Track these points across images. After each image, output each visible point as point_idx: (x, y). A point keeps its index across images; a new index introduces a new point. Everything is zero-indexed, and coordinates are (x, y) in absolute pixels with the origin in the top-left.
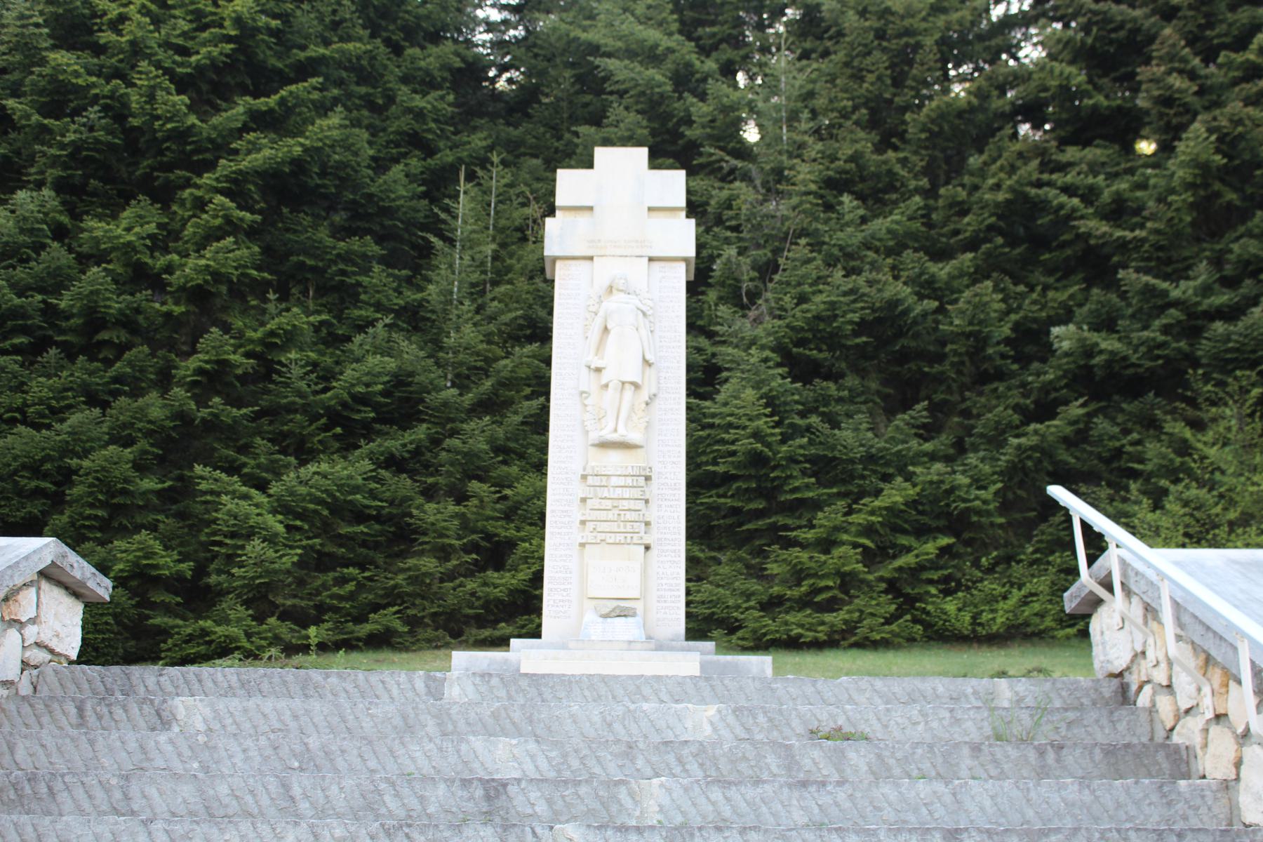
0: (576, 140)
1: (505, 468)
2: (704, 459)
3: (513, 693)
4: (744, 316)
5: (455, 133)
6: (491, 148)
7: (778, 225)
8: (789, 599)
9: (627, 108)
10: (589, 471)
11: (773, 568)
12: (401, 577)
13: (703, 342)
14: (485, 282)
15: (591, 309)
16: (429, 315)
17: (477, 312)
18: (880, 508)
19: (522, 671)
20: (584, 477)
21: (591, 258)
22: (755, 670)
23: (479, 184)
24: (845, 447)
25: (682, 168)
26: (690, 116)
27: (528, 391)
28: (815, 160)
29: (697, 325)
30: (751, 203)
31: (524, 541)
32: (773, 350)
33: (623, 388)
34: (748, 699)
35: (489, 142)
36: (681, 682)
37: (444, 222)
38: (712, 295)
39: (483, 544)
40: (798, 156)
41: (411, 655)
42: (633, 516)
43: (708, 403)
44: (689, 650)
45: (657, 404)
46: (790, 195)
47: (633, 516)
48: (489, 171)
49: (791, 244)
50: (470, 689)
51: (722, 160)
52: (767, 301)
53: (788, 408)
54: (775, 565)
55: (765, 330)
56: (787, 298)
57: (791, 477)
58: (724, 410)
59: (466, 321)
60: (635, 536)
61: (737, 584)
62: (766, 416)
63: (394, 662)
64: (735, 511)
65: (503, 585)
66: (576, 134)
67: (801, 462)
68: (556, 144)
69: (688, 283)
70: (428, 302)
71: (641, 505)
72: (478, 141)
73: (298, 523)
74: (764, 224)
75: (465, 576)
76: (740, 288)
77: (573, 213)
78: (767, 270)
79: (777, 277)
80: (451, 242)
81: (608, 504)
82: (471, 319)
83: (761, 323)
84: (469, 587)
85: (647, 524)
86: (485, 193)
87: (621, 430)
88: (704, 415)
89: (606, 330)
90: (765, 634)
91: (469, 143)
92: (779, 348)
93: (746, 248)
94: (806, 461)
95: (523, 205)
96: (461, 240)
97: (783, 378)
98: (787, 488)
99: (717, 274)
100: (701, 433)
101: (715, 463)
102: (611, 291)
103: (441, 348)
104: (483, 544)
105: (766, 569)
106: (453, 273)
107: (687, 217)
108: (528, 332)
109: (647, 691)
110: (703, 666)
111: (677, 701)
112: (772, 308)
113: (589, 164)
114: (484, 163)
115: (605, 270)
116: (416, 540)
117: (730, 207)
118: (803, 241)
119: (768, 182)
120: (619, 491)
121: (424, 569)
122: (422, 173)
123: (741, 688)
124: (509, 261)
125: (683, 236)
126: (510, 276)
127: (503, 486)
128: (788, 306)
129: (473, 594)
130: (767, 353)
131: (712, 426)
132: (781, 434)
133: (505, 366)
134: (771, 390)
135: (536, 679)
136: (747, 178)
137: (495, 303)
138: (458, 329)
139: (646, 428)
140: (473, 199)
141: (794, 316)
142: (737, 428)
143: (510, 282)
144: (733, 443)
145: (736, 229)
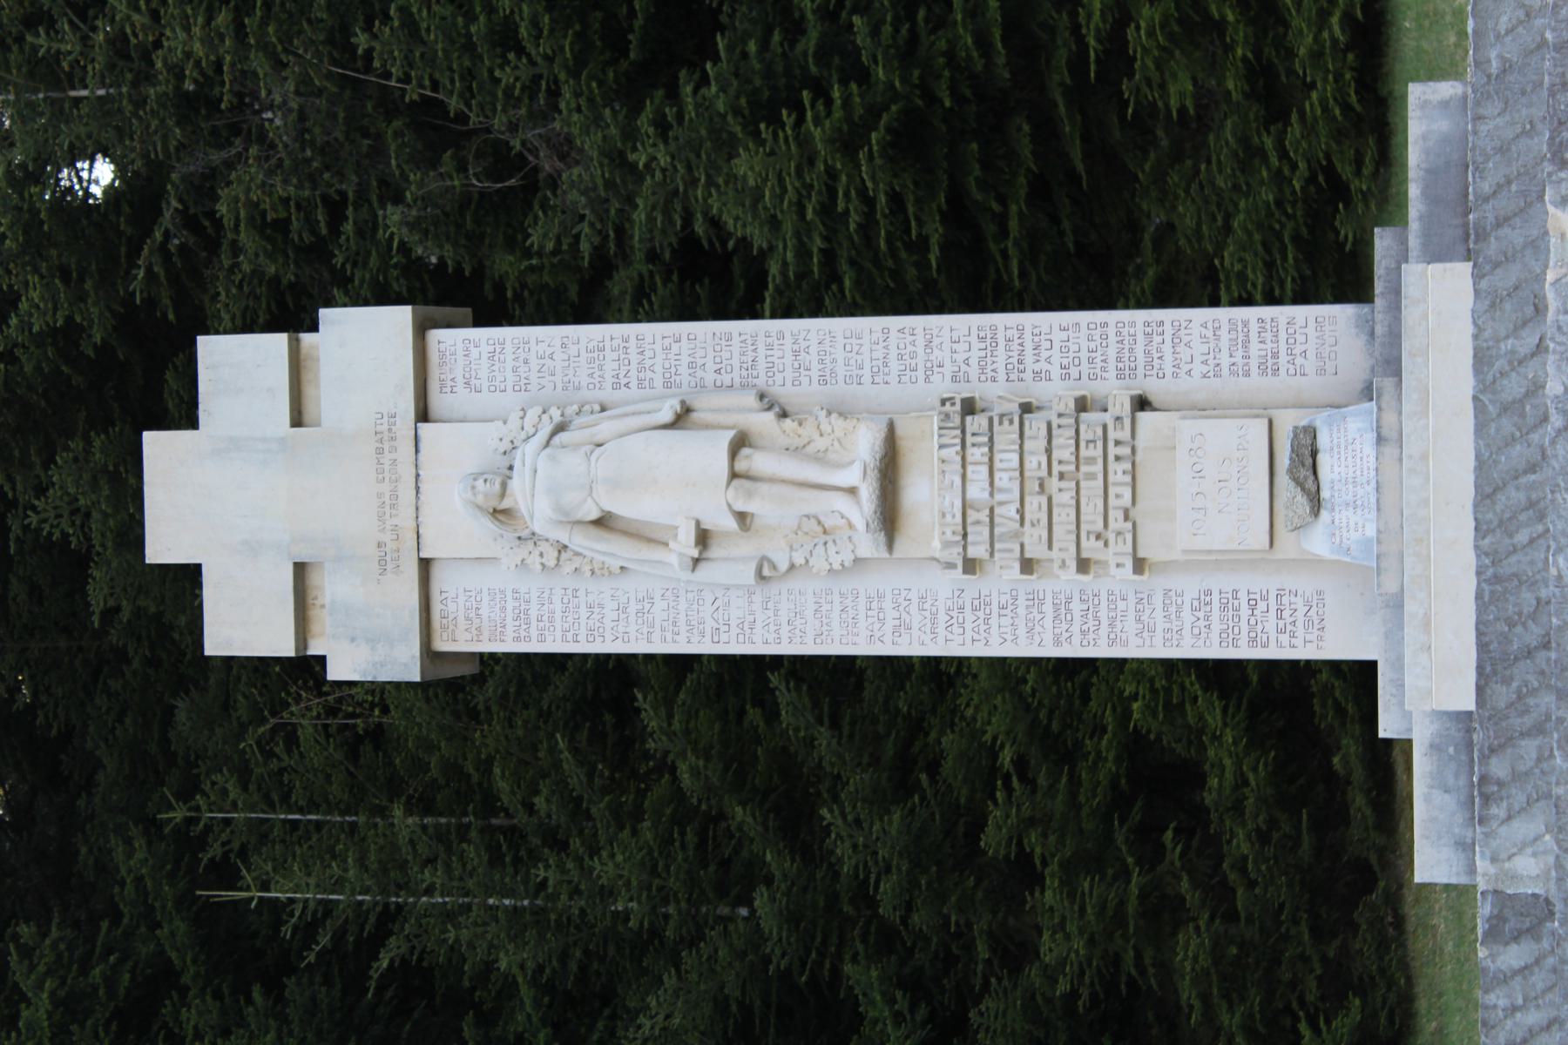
0: (125, 615)
1: (948, 766)
2: (911, 273)
3: (1528, 721)
4: (554, 182)
5: (116, 917)
6: (152, 827)
7: (322, 103)
8: (1258, 53)
9: (41, 491)
10: (955, 555)
11: (1180, 91)
12: (1225, 1019)
13: (620, 284)
14: (487, 830)
15: (551, 557)
16: (573, 966)
17: (563, 846)
19: (1470, 705)
20: (970, 566)
21: (425, 565)
22: (1443, 125)
23: (243, 853)
25: (194, 343)
26: (54, 332)
27: (754, 714)
28: (155, 16)
29: (579, 298)
30: (270, 173)
31: (1127, 714)
32: (636, 109)
33: (747, 476)
34: (1530, 132)
35: (134, 831)
36: (1488, 302)
37: (339, 936)
38: (505, 264)
39: (1136, 815)
40: (147, 59)
41: (1421, 987)
42: (1063, 440)
43: (774, 268)
44: (1397, 291)
45: (783, 390)
46: (247, 75)
47: (1063, 440)
48: (208, 828)
49: (368, 69)
50: (1522, 828)
51: (163, 248)
52: (513, 128)
53: (780, 68)
54: (1172, 89)
55: (586, 131)
56: (505, 76)
57: (950, 55)
58: (788, 227)
59: (586, 872)
60: (1112, 435)
61: (1220, 182)
62: (800, 121)
63: (1439, 1030)
64: (1040, 190)
65: (1238, 764)
66: (110, 614)
67: (913, 33)
68: (136, 664)
69: (479, 322)
70: (540, 969)
71: (1036, 425)
72: (133, 859)
74: (319, 141)
75: (1220, 859)
76: (483, 194)
77: (314, 613)
78: (436, 130)
79: (454, 104)
80: (389, 918)
81: (1035, 504)
82: (579, 860)
83: (569, 140)
84: (1245, 848)
85: (1082, 405)
86: (264, 838)
87: (851, 477)
88: (801, 276)
89: (603, 522)
90: (1346, 107)
91: (139, 880)
92: (630, 95)
93: (383, 183)
94: (911, 17)
95: (292, 739)
96: (384, 891)
97: (704, 81)
98: (979, 66)
99: (449, 251)
100: (847, 283)
101: (922, 245)
102: (505, 512)
103: (655, 933)
104: (1136, 815)
105: (1182, 111)
106: (468, 908)
107: (314, 328)
108: (608, 718)
109: (1513, 387)
110: (1435, 254)
111: (1540, 309)
112: (531, 115)
113: (190, 575)
114: (189, 840)
115: (454, 528)
116: (1132, 983)
117: (283, 226)
118: (361, 40)
119: (214, 132)
120: (1002, 479)
121: (1205, 961)
122: (218, 995)
123: (1503, 150)
124: (434, 772)
125: (364, 341)
126: (469, 768)
127: (994, 770)
128: (525, 73)
129: (1263, 837)
130: (644, 123)
131: (829, 256)
132: (844, 82)
133: (695, 772)
134: (737, 112)
135: (1492, 665)
136: (206, 186)
137: (539, 802)
138: (607, 893)
140: (281, 866)
141: (549, 59)
142: (832, 193)
143: (486, 766)
144: (869, 202)
145: (336, 211)
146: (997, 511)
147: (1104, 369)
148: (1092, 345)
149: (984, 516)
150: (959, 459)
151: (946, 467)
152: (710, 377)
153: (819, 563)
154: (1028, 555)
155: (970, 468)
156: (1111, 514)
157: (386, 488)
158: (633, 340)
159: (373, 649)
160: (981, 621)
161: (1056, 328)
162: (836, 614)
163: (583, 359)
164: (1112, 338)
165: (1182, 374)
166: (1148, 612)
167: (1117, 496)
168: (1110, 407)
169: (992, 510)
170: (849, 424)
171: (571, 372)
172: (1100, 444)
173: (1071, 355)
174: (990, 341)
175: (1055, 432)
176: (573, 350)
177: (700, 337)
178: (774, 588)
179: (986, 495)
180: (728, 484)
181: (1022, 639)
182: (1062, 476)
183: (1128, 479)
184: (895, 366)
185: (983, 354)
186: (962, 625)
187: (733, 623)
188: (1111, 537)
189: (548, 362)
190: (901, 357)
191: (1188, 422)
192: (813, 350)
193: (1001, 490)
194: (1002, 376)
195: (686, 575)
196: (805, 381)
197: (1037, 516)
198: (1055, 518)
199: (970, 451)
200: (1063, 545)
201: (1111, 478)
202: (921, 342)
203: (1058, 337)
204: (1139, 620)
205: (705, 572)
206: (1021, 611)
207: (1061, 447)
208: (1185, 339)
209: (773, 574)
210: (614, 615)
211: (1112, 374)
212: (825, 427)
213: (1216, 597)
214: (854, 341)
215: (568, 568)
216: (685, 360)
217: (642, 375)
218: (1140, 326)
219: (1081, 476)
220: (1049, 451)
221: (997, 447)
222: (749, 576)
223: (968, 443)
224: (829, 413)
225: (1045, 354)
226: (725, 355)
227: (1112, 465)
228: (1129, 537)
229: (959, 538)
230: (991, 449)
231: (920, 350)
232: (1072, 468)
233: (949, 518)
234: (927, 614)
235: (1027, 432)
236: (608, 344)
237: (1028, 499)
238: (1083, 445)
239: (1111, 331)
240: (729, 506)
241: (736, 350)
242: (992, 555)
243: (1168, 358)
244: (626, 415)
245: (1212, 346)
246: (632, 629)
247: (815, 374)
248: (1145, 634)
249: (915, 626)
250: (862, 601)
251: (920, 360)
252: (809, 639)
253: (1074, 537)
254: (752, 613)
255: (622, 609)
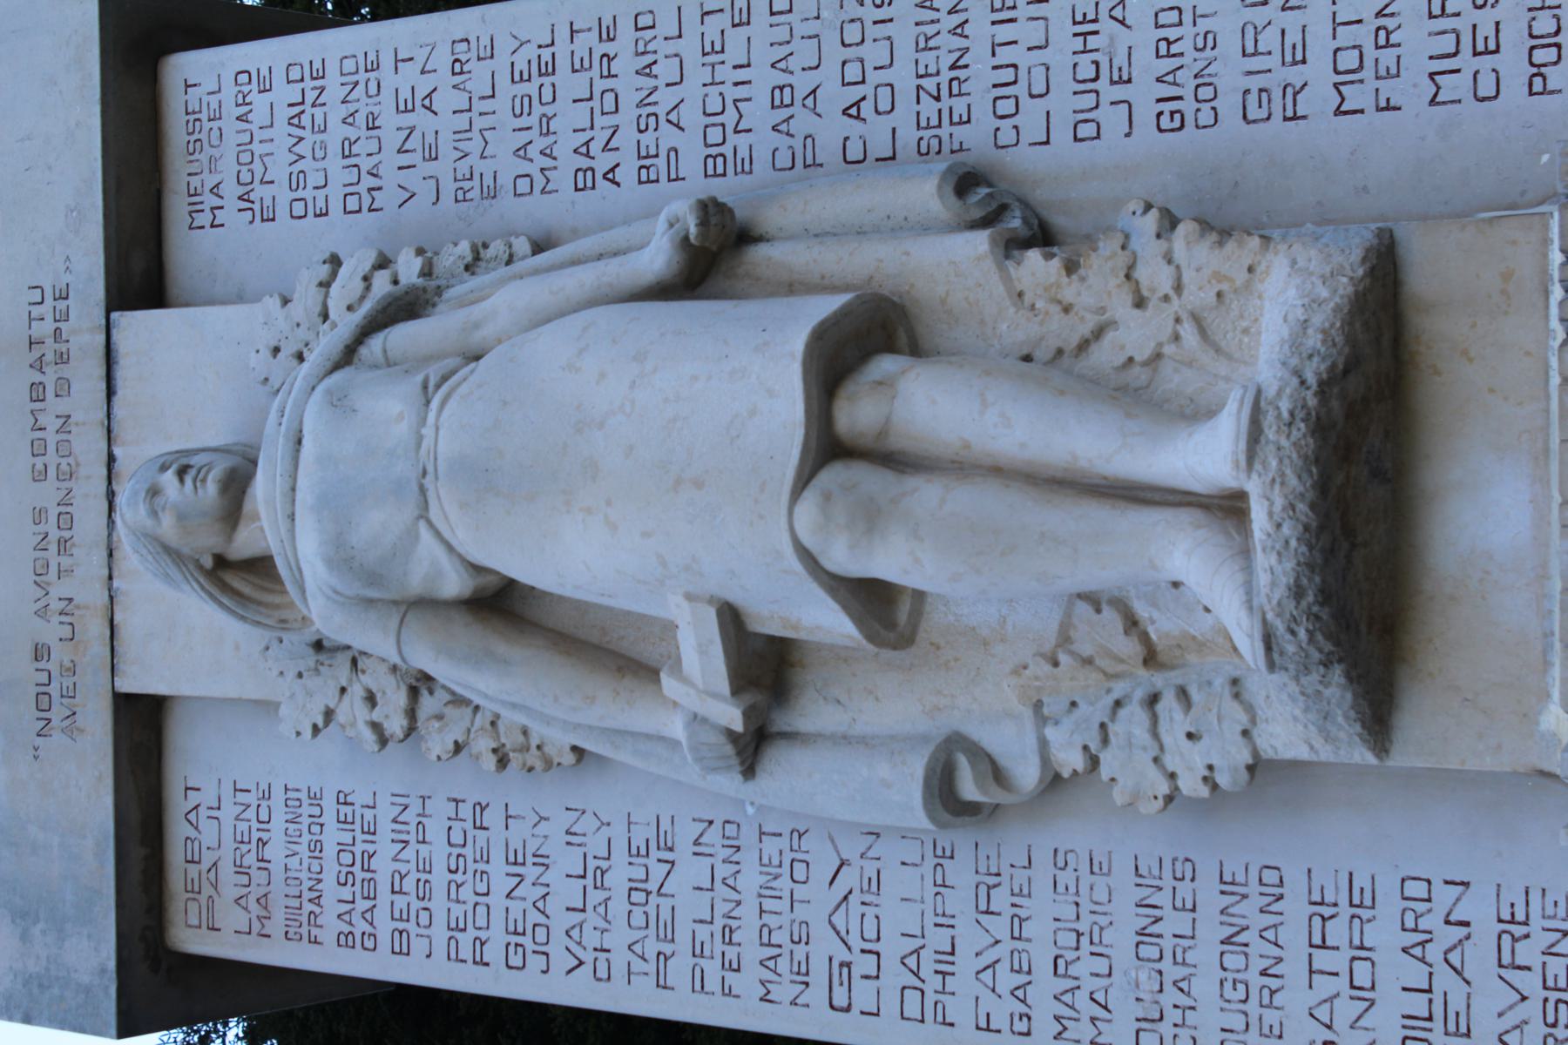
33: (891, 459)
45: (1044, 163)
87: (1206, 455)
139: (1218, 229)
152: (830, 130)
153: (1129, 768)
157: (48, 495)
159: (25, 937)
162: (1205, 954)
163: (502, 104)
170: (1236, 256)
171: (475, 146)
176: (479, 79)
178: (1011, 843)
180: (803, 481)
187: (892, 948)
189: (420, 118)
196: (1113, 120)
205: (790, 779)
209: (997, 796)
210: (571, 893)
212: (1155, 276)
215: (437, 742)
216: (763, 79)
217: (648, 139)
224: (1170, 221)
226: (875, 53)
234: (1530, 983)
236: (563, 49)
240: (808, 558)
244: (576, 262)
246: (618, 939)
247: (1144, 94)
250: (1295, 908)
254: (945, 922)
255: (593, 875)
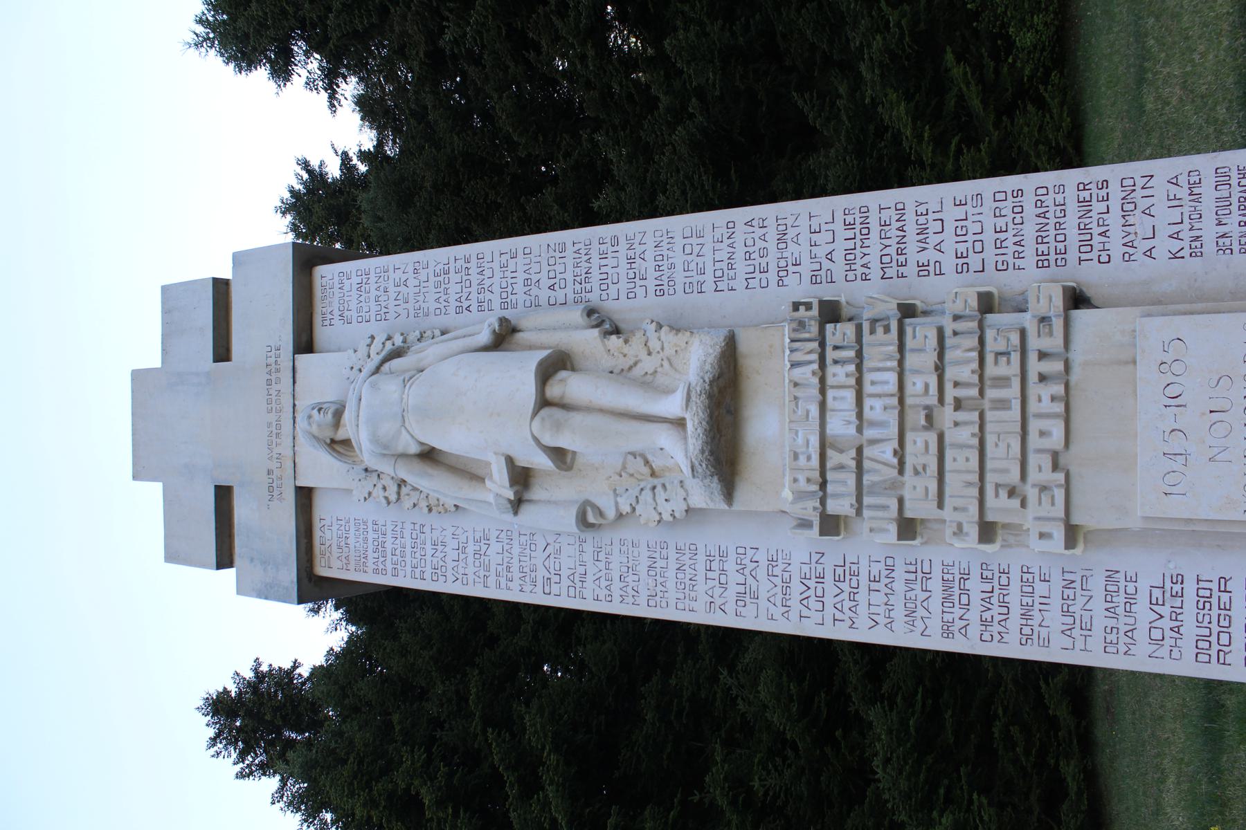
10: (810, 509)
18: (914, 129)
20: (830, 525)
24: (846, 178)
45: (617, 306)
60: (1034, 343)
71: (922, 333)
73: (942, 791)
81: (920, 444)
85: (987, 304)
87: (672, 406)
102: (346, 443)
120: (875, 408)
139: (676, 329)
146: (867, 452)
147: (1018, 256)
148: (1001, 223)
149: (848, 458)
150: (816, 381)
151: (799, 393)
152: (544, 294)
153: (646, 511)
154: (909, 514)
155: (830, 394)
156: (1033, 460)
158: (474, 260)
159: (265, 570)
160: (845, 596)
161: (948, 203)
162: (671, 573)
163: (431, 284)
164: (1030, 210)
165: (1139, 256)
166: (1081, 601)
167: (1042, 434)
168: (1032, 304)
169: (860, 451)
171: (421, 298)
172: (1015, 357)
173: (970, 238)
174: (859, 227)
175: (949, 342)
177: (536, 251)
178: (606, 537)
179: (852, 430)
180: (535, 414)
181: (899, 625)
182: (958, 405)
183: (1059, 408)
184: (741, 267)
185: (850, 244)
186: (820, 599)
187: (565, 573)
188: (1032, 493)
189: (402, 288)
190: (748, 256)
191: (1158, 321)
192: (649, 256)
193: (873, 424)
194: (875, 272)
195: (509, 517)
196: (640, 292)
197: (922, 460)
198: (949, 465)
199: (831, 369)
200: (959, 503)
201: (1033, 407)
202: (772, 235)
203: (952, 214)
204: (1066, 613)
206: (899, 586)
207: (958, 363)
208: (1143, 204)
210: (454, 555)
211: (1030, 260)
212: (654, 344)
213: (1190, 588)
214: (694, 241)
215: (407, 503)
216: (521, 276)
217: (481, 296)
218: (1071, 192)
219: (986, 404)
220: (940, 369)
221: (867, 364)
222: (570, 516)
223: (829, 360)
224: (660, 326)
225: (933, 240)
227: (1034, 389)
228: (1060, 495)
229: (815, 488)
230: (859, 367)
231: (772, 245)
232: (974, 392)
233: (802, 460)
234: (778, 581)
235: (910, 343)
236: (452, 265)
237: (909, 436)
238: (990, 358)
239: (1029, 201)
241: (570, 262)
242: (859, 512)
243: (1116, 233)
245: (1186, 210)
246: (470, 570)
247: (651, 284)
248: (1076, 632)
249: (763, 595)
250: (701, 558)
251: (772, 259)
252: (642, 599)
253: (975, 492)
255: (462, 549)
